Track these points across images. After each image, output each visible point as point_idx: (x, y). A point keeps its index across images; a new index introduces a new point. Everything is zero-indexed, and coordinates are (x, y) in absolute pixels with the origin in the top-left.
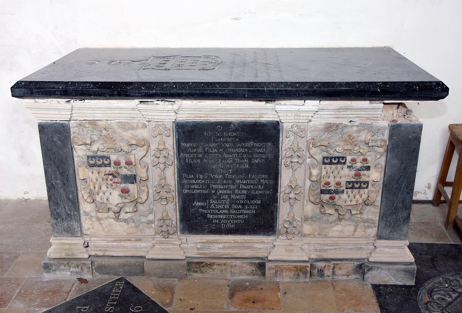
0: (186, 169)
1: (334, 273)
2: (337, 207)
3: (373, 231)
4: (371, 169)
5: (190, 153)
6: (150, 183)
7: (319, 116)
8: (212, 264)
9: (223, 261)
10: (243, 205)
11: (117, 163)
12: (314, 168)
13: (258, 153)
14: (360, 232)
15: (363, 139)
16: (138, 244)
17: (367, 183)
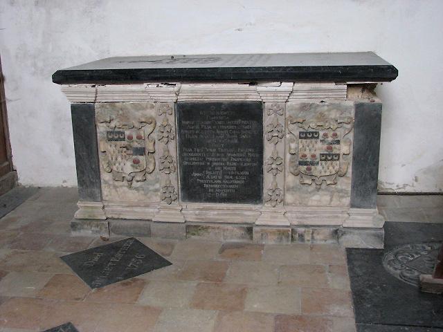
0: (186, 144)
1: (313, 238)
2: (314, 178)
3: (347, 201)
4: (342, 143)
5: (189, 130)
6: (156, 156)
7: (294, 97)
8: (207, 228)
9: (217, 226)
10: (234, 175)
11: (130, 138)
12: (292, 142)
13: (245, 130)
14: (335, 202)
15: (333, 116)
16: (147, 210)
17: (339, 155)
